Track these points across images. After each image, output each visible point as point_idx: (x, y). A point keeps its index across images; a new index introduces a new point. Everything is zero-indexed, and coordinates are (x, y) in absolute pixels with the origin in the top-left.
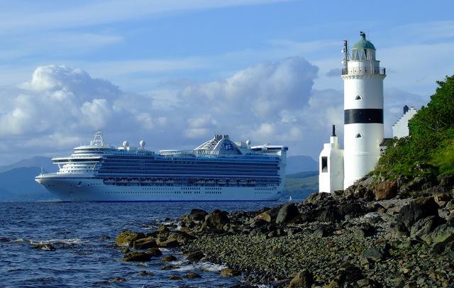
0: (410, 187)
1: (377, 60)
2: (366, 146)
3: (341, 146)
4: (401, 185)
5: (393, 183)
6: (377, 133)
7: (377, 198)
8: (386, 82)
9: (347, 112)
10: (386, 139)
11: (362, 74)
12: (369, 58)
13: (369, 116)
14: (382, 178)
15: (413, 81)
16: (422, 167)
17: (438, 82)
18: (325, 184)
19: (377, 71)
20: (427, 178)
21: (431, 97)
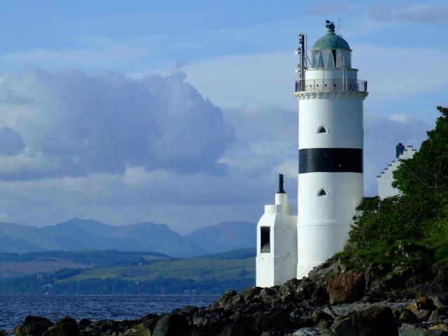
0: (387, 282)
1: (353, 67)
2: (334, 210)
3: (293, 210)
4: (372, 279)
5: (357, 276)
6: (352, 188)
7: (332, 301)
8: (366, 103)
9: (303, 153)
10: (367, 199)
11: (327, 91)
12: (340, 63)
13: (338, 160)
14: (342, 266)
15: (399, 113)
16: (408, 249)
17: (440, 108)
18: (265, 275)
19: (353, 85)
20: (415, 268)
21: (429, 133)
